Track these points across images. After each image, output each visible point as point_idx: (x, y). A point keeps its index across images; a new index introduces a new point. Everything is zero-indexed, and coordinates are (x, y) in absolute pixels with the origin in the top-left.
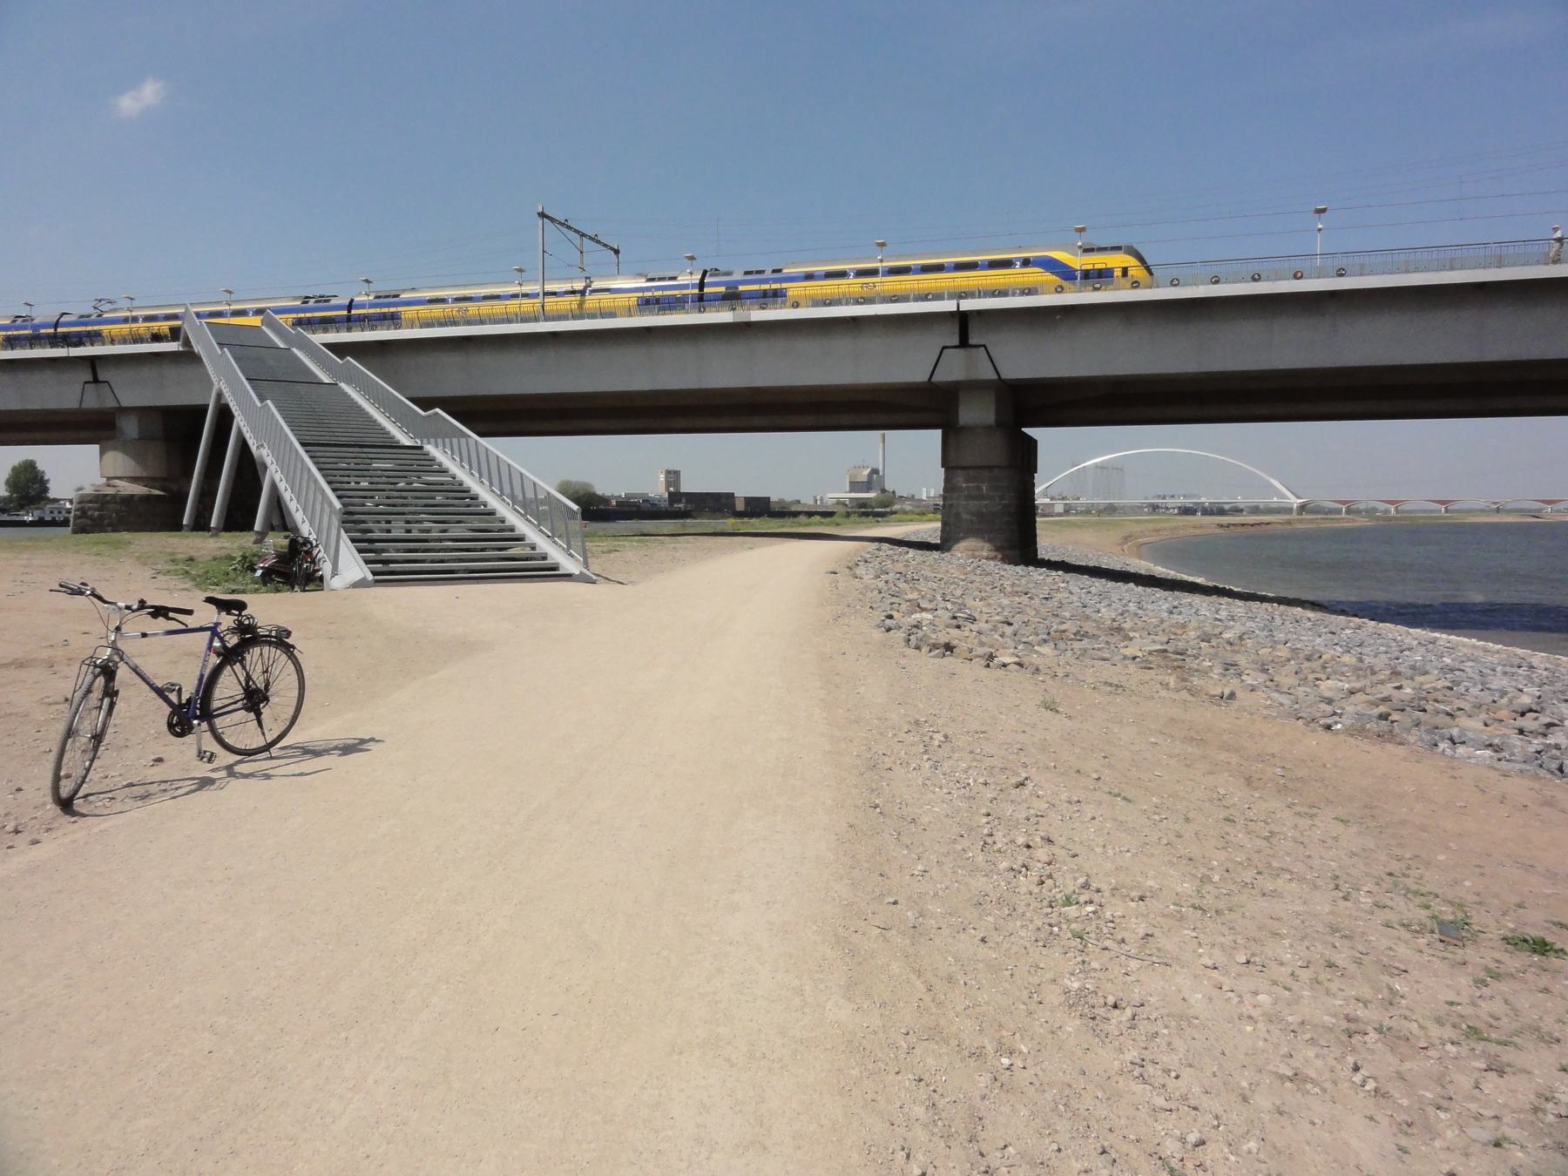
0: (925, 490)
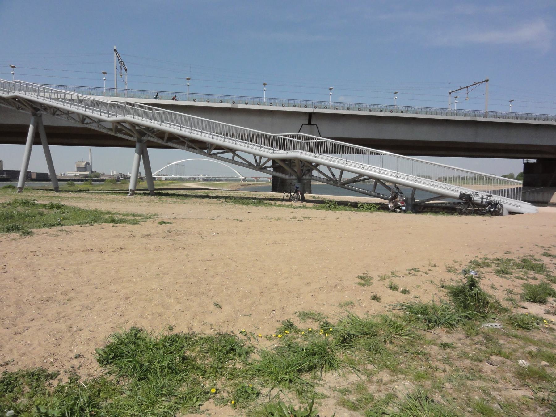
0: (112, 171)
